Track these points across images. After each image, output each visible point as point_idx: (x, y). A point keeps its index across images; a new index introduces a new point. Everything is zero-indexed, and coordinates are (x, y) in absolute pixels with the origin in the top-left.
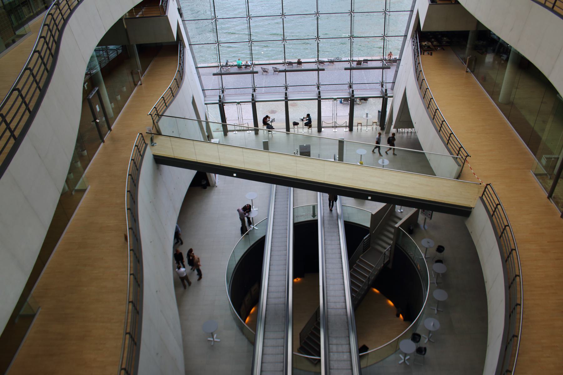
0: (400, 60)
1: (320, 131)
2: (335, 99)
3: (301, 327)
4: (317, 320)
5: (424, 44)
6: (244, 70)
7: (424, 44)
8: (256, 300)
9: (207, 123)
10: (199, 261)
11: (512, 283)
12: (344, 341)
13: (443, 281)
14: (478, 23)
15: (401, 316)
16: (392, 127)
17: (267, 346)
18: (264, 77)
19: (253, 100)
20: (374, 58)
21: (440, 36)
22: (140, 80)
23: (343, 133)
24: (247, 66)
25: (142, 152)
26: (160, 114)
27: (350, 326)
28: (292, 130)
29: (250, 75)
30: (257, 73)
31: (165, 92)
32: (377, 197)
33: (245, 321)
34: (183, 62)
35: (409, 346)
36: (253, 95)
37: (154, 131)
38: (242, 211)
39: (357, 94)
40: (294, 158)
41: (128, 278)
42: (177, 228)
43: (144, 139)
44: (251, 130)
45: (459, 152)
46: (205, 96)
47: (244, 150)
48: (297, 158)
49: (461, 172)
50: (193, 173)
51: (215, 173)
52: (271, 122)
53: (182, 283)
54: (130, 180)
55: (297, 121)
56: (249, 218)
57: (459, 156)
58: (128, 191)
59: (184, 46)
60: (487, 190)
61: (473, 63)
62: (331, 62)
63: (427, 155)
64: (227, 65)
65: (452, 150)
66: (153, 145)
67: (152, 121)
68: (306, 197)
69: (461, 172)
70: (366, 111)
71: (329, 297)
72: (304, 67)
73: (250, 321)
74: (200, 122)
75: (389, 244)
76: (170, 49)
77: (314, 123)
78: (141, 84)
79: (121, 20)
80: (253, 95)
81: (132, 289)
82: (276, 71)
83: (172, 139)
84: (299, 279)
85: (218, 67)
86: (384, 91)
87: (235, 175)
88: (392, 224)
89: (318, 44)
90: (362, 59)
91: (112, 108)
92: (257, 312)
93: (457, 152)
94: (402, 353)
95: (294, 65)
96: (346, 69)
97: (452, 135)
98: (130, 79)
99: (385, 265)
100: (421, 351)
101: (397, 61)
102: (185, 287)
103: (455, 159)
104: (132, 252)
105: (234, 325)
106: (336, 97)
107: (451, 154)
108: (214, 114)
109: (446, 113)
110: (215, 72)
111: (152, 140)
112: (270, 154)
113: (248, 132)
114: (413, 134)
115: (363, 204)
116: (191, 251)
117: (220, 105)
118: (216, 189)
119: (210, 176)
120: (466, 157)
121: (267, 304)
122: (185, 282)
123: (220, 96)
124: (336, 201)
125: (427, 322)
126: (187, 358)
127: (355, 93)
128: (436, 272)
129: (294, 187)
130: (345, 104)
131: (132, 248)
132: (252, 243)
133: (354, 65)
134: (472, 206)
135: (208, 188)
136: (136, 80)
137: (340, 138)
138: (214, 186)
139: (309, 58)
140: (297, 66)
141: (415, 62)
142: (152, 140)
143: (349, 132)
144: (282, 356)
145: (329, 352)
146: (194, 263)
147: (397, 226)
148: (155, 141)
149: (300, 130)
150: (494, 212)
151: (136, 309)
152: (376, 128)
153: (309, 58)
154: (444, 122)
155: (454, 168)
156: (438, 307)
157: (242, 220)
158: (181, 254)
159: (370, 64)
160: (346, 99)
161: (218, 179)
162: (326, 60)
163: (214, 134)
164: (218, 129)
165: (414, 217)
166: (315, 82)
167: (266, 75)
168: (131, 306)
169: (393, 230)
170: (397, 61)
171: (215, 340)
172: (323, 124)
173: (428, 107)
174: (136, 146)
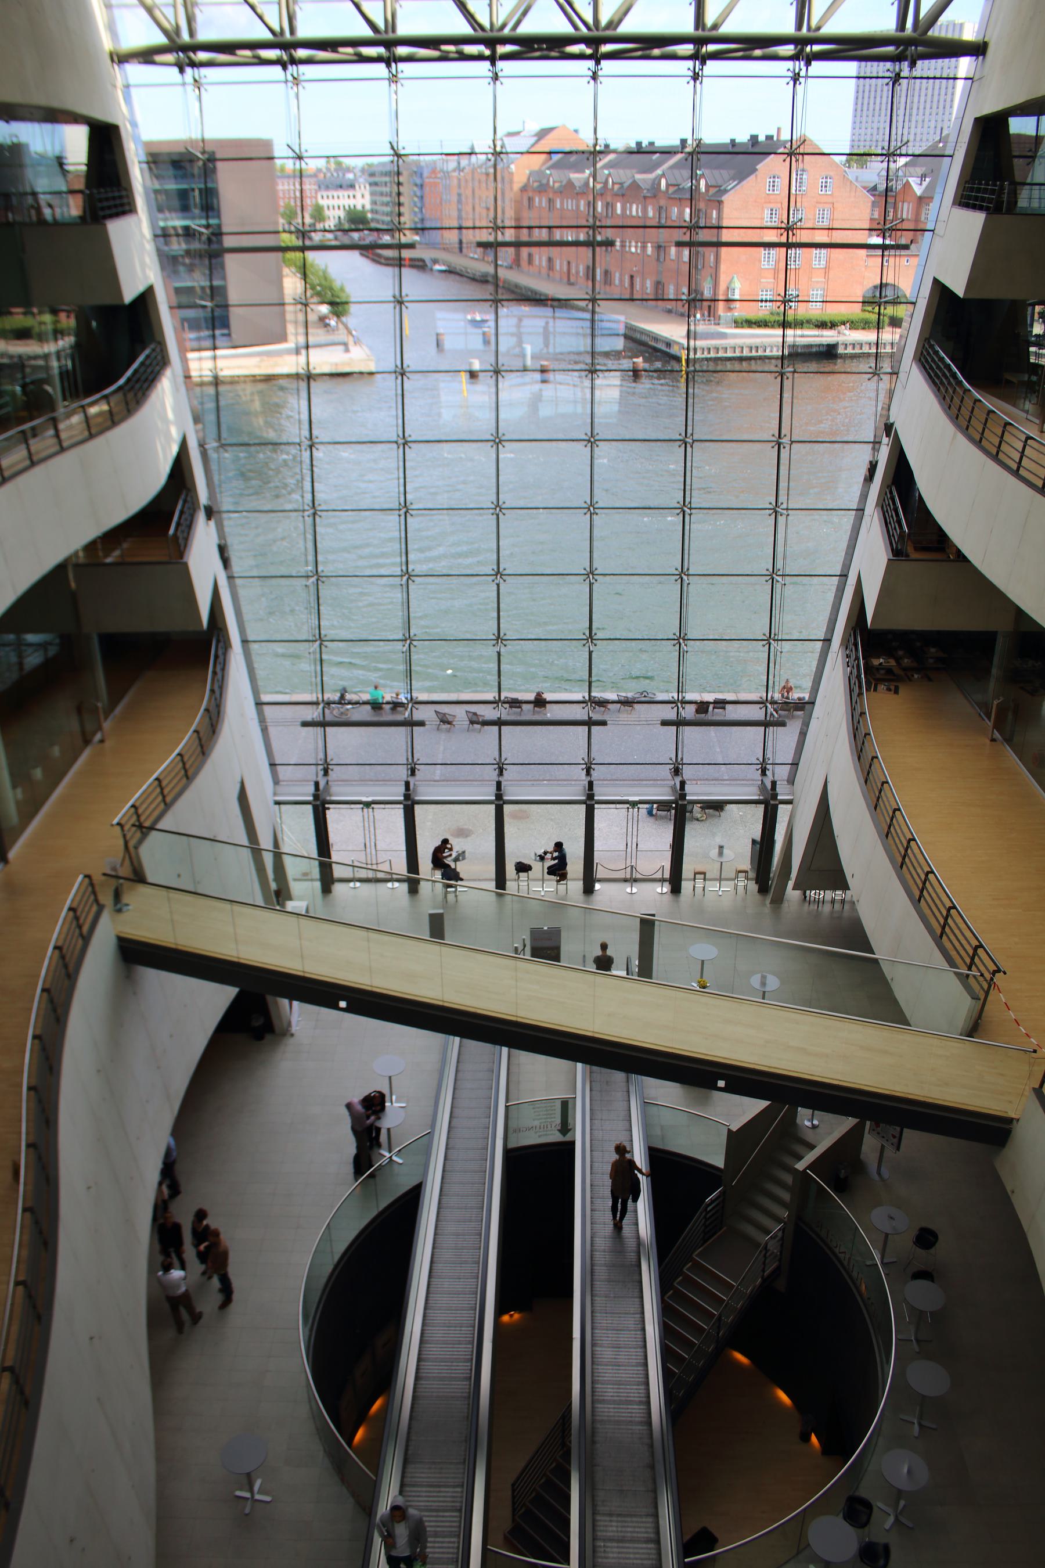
0: (813, 703)
1: (588, 889)
2: (634, 804)
5: (876, 662)
6: (388, 715)
7: (876, 662)
9: (278, 856)
13: (934, 1336)
14: (1019, 613)
15: (814, 1439)
16: (791, 884)
18: (443, 736)
19: (407, 797)
20: (743, 697)
21: (918, 644)
23: (653, 897)
24: (396, 705)
26: (147, 824)
27: (660, 1468)
29: (402, 730)
30: (421, 724)
33: (350, 1443)
34: (221, 687)
35: (835, 1538)
37: (125, 871)
38: (359, 1108)
39: (695, 792)
42: (168, 1153)
43: (94, 893)
45: (972, 959)
46: (276, 782)
47: (373, 935)
48: (521, 964)
50: (230, 993)
51: (292, 998)
52: (456, 860)
53: (173, 1319)
57: (974, 972)
58: (35, 1037)
59: (227, 645)
61: (1010, 716)
62: (627, 703)
63: (885, 968)
64: (342, 701)
65: (953, 953)
66: (119, 911)
67: (121, 842)
68: (544, 1076)
70: (718, 840)
71: (600, 1369)
72: (552, 713)
73: (364, 1440)
75: (779, 1220)
76: (192, 651)
77: (575, 866)
78: (102, 741)
79: (60, 569)
80: (407, 784)
81: (15, 1328)
82: (475, 720)
83: (174, 895)
85: (317, 703)
86: (769, 786)
87: (343, 1004)
88: (788, 1160)
89: (590, 653)
90: (709, 697)
91: (18, 803)
92: (386, 1409)
93: (968, 960)
95: (524, 706)
96: (665, 723)
97: (953, 911)
98: (74, 724)
101: (805, 706)
102: (180, 1327)
103: (964, 979)
106: (636, 799)
107: (952, 963)
108: (297, 833)
109: (940, 849)
110: (309, 718)
111: (117, 896)
113: (390, 885)
114: (846, 907)
115: (704, 1102)
116: (201, 1215)
118: (291, 1041)
119: (276, 1003)
120: (994, 973)
122: (183, 1311)
123: (317, 784)
124: (635, 1200)
125: (894, 1465)
127: (688, 788)
129: (510, 1045)
130: (662, 818)
131: (29, 1204)
132: (384, 1204)
133: (689, 712)
134: (1014, 1116)
135: (268, 1037)
137: (642, 910)
138: (286, 1032)
141: (853, 709)
143: (669, 897)
146: (214, 1256)
147: (800, 1166)
148: (126, 899)
149: (536, 887)
151: (22, 1392)
154: (931, 876)
155: (963, 1006)
156: (921, 1417)
158: (177, 1228)
159: (733, 713)
160: (663, 805)
161: (299, 1015)
162: (612, 696)
164: (305, 874)
165: (850, 1142)
166: (581, 755)
167: (449, 731)
169: (788, 1179)
170: (805, 706)
171: (257, 1497)
172: (600, 873)
173: (887, 833)
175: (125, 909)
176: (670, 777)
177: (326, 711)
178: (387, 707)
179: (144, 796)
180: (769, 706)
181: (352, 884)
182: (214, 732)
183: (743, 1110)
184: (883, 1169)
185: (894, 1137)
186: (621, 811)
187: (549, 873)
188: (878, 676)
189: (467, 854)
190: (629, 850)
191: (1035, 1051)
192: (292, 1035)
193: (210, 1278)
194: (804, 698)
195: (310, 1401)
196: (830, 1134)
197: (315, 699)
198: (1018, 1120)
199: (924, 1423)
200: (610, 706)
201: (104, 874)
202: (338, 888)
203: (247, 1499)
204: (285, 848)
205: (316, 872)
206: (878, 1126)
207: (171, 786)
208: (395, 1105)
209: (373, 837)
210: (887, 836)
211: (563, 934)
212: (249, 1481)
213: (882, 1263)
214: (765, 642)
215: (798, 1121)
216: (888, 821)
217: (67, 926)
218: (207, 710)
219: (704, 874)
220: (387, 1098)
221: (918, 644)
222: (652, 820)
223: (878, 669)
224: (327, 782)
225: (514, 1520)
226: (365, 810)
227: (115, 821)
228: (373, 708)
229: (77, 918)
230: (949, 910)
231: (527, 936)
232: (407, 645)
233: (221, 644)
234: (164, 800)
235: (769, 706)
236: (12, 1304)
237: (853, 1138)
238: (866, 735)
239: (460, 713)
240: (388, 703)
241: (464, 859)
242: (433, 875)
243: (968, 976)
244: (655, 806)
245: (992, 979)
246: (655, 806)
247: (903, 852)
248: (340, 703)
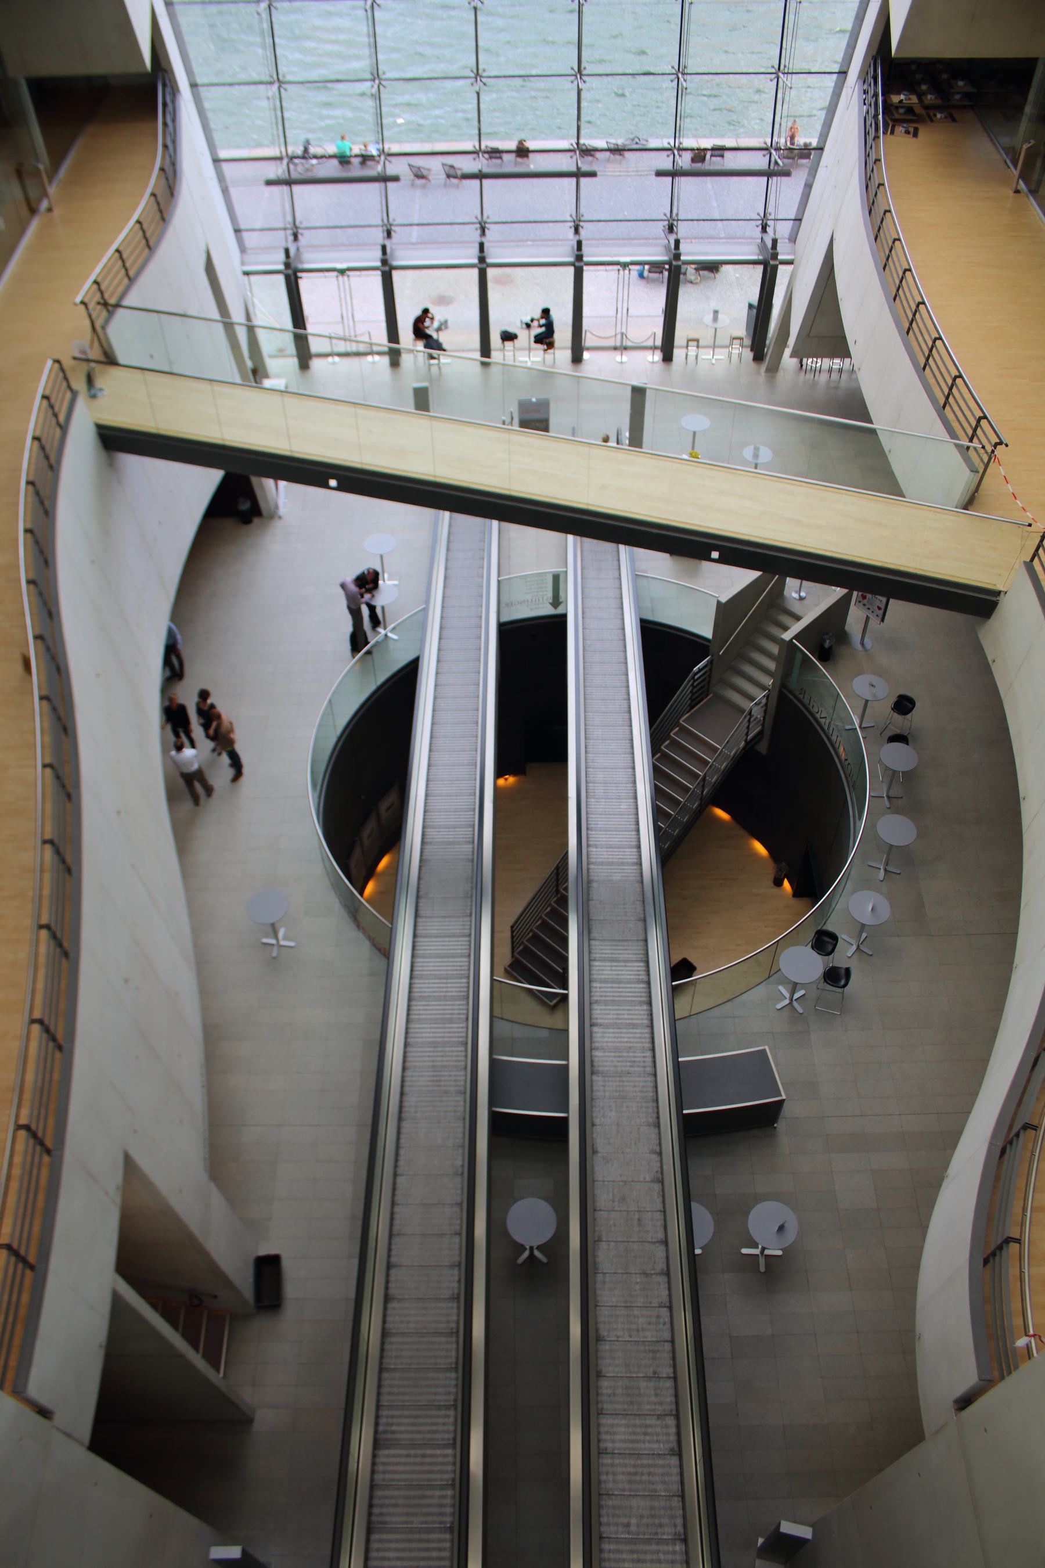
0: (822, 149)
1: (577, 359)
2: (625, 265)
3: (515, 908)
4: (558, 891)
5: (895, 99)
6: (355, 170)
7: (895, 99)
8: (393, 836)
9: (251, 330)
10: (231, 730)
12: (632, 951)
13: (906, 793)
15: (786, 884)
16: (787, 352)
17: (422, 977)
18: (418, 193)
19: (384, 262)
20: (744, 143)
21: (945, 76)
22: (45, 194)
23: (644, 366)
24: (365, 159)
25: (62, 418)
28: (496, 356)
29: (376, 186)
30: (396, 179)
31: (124, 234)
32: (735, 552)
33: (361, 893)
34: (174, 142)
35: (804, 964)
36: (384, 248)
37: (95, 353)
38: (353, 588)
39: (691, 252)
40: (505, 436)
41: (39, 776)
42: (171, 634)
43: (66, 378)
44: (379, 353)
45: (975, 430)
46: (243, 249)
47: (360, 411)
48: (514, 437)
49: (977, 490)
50: (212, 477)
51: (277, 476)
52: (439, 330)
53: (189, 789)
54: (30, 499)
55: (511, 330)
56: (372, 608)
57: (975, 444)
59: (175, 91)
62: (617, 151)
63: (883, 438)
64: (306, 155)
65: (955, 425)
66: (94, 397)
67: (88, 323)
68: (536, 549)
69: (977, 490)
70: (713, 305)
72: (535, 163)
74: (229, 327)
75: (763, 688)
77: (563, 334)
78: (50, 210)
80: (384, 248)
82: (452, 174)
84: (511, 780)
85: (281, 159)
86: (769, 244)
87: (333, 483)
88: (774, 631)
90: (707, 143)
92: (395, 868)
93: (970, 432)
94: (785, 981)
95: (505, 156)
96: (660, 174)
99: (750, 747)
100: (835, 977)
102: (196, 800)
103: (964, 450)
104: (45, 703)
105: (333, 901)
106: (628, 259)
107: (953, 434)
108: (269, 305)
110: (272, 176)
111: (90, 380)
112: (436, 424)
113: (370, 358)
115: (694, 574)
117: (288, 278)
119: (262, 486)
120: (996, 445)
122: (198, 786)
125: (858, 901)
126: (205, 991)
128: (887, 769)
129: (501, 518)
130: (654, 281)
132: (382, 678)
133: (685, 161)
134: (1001, 588)
135: (256, 521)
136: (33, 194)
138: (273, 515)
139: (551, 141)
140: (514, 163)
142: (90, 380)
143: (660, 366)
144: (470, 846)
145: (589, 900)
146: (222, 739)
148: (99, 383)
151: (63, 861)
152: (740, 356)
153: (551, 141)
155: (961, 478)
156: (887, 864)
157: (355, 614)
158: (182, 709)
159: (732, 161)
160: (656, 267)
161: (283, 495)
162: (601, 144)
163: (272, 365)
164: (281, 350)
165: (837, 612)
166: (567, 212)
167: (424, 187)
168: (49, 852)
169: (775, 649)
171: (282, 943)
172: (588, 340)
175: (99, 394)
176: (663, 235)
177: (291, 167)
178: (356, 161)
179: (106, 270)
180: (773, 152)
181: (330, 359)
182: (172, 194)
183: (733, 580)
184: (867, 640)
185: (879, 608)
186: (612, 272)
187: (536, 342)
188: (897, 116)
189: (449, 323)
190: (619, 315)
191: (1030, 525)
192: (280, 517)
193: (220, 754)
194: (810, 144)
195: (323, 860)
196: (816, 605)
197: (278, 154)
199: (889, 868)
200: (598, 155)
201: (75, 358)
202: (316, 364)
203: (273, 945)
204: (258, 321)
205: (291, 348)
206: (864, 597)
207: (133, 258)
208: (387, 582)
209: (349, 308)
210: (895, 299)
211: (553, 407)
212: (274, 930)
213: (860, 727)
214: (773, 76)
215: (786, 593)
216: (898, 283)
217: (42, 415)
218: (162, 169)
219: (698, 341)
220: (380, 577)
221: (945, 76)
222: (642, 283)
223: (897, 108)
224: (298, 249)
225: (513, 956)
226: (341, 278)
227: (78, 299)
228: (341, 163)
229: (52, 407)
231: (514, 409)
232: (376, 87)
233: (168, 90)
234: (127, 275)
235: (773, 152)
236: (43, 786)
237: (840, 609)
238: (879, 185)
239: (435, 166)
240: (356, 156)
241: (446, 328)
242: (415, 346)
243: (968, 448)
244: (647, 267)
245: (993, 452)
246: (647, 267)
247: (910, 316)
248: (304, 157)
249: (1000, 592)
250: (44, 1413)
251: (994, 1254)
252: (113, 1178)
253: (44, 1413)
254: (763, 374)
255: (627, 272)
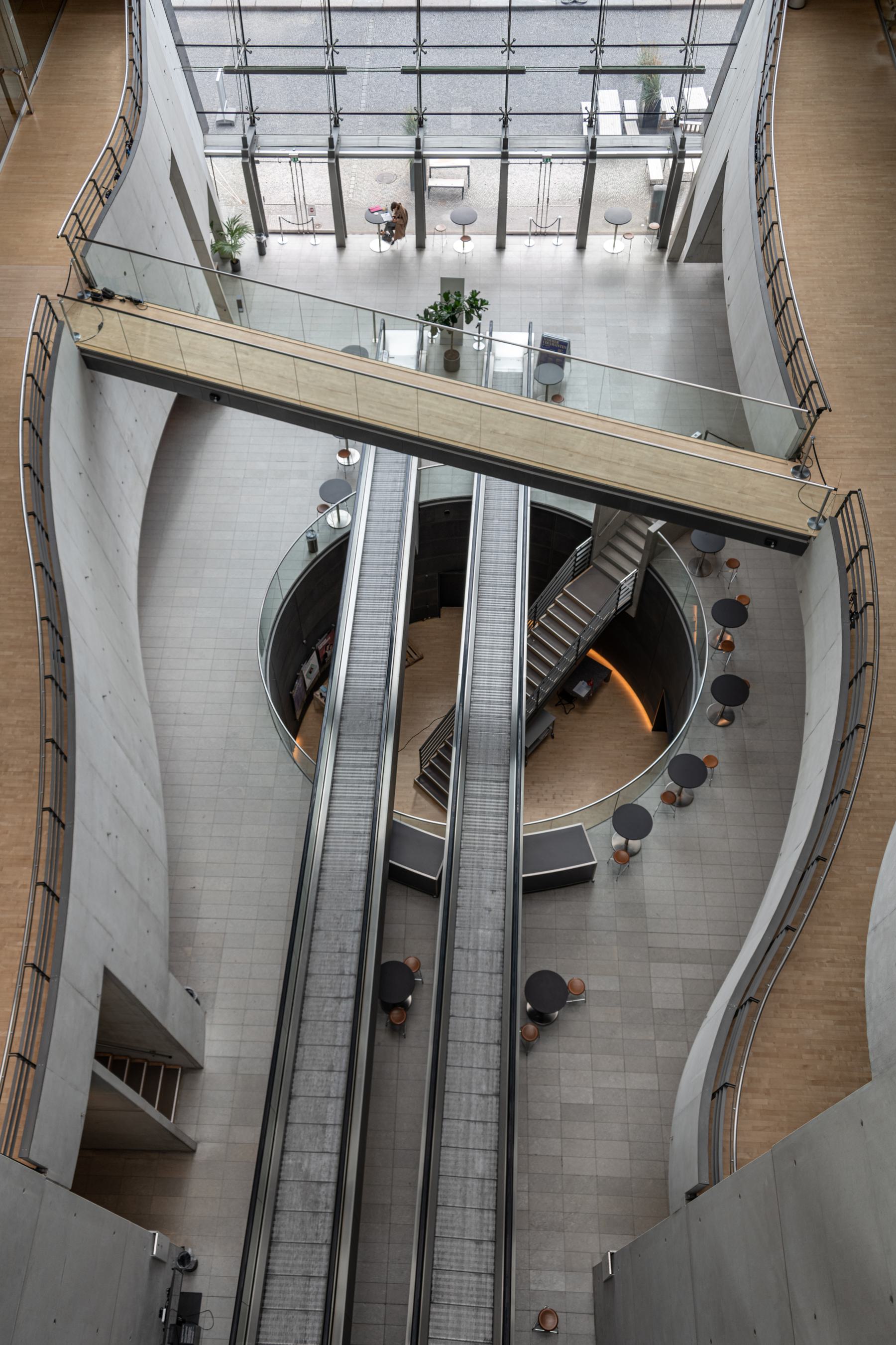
11: (856, 677)
60: (844, 509)
78: (30, 113)
117: (245, 165)
121: (345, 690)
150: (852, 562)
155: (792, 433)
174: (27, 375)
198: (815, 538)
230: (797, 341)
249: (810, 537)
250: (40, 1169)
251: (718, 1091)
252: (94, 990)
253: (40, 1169)
254: (665, 262)
255: (548, 165)
